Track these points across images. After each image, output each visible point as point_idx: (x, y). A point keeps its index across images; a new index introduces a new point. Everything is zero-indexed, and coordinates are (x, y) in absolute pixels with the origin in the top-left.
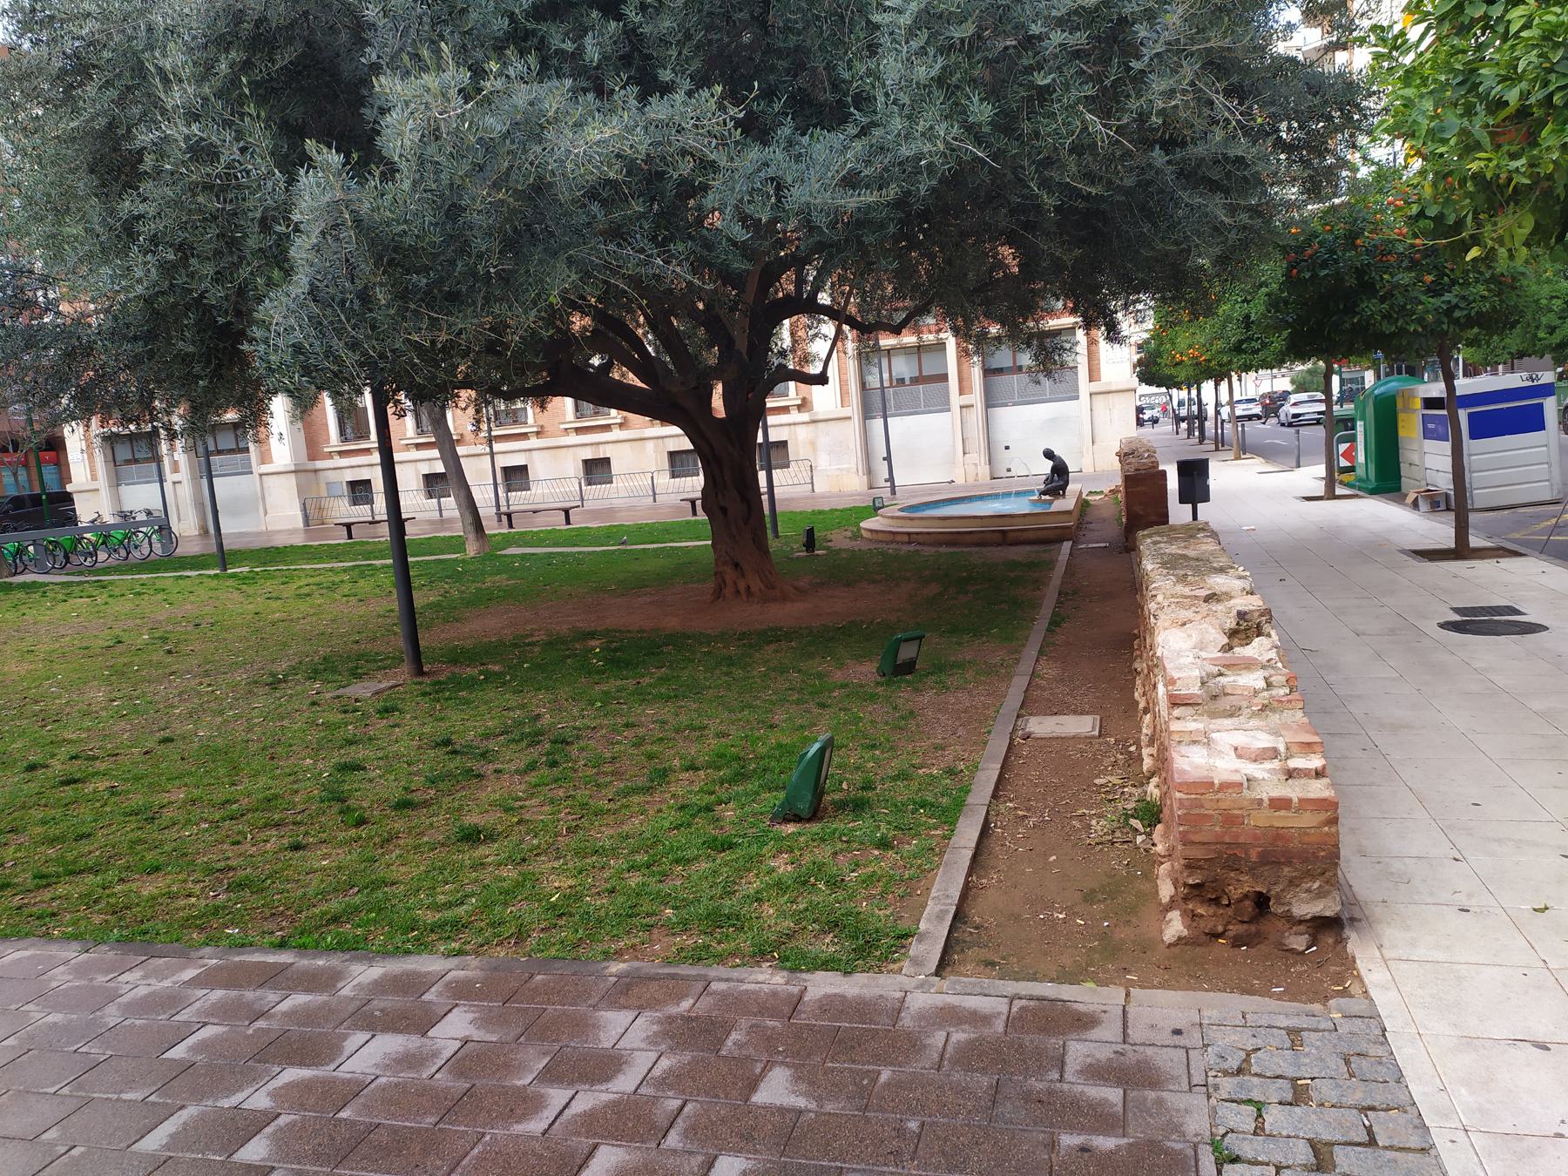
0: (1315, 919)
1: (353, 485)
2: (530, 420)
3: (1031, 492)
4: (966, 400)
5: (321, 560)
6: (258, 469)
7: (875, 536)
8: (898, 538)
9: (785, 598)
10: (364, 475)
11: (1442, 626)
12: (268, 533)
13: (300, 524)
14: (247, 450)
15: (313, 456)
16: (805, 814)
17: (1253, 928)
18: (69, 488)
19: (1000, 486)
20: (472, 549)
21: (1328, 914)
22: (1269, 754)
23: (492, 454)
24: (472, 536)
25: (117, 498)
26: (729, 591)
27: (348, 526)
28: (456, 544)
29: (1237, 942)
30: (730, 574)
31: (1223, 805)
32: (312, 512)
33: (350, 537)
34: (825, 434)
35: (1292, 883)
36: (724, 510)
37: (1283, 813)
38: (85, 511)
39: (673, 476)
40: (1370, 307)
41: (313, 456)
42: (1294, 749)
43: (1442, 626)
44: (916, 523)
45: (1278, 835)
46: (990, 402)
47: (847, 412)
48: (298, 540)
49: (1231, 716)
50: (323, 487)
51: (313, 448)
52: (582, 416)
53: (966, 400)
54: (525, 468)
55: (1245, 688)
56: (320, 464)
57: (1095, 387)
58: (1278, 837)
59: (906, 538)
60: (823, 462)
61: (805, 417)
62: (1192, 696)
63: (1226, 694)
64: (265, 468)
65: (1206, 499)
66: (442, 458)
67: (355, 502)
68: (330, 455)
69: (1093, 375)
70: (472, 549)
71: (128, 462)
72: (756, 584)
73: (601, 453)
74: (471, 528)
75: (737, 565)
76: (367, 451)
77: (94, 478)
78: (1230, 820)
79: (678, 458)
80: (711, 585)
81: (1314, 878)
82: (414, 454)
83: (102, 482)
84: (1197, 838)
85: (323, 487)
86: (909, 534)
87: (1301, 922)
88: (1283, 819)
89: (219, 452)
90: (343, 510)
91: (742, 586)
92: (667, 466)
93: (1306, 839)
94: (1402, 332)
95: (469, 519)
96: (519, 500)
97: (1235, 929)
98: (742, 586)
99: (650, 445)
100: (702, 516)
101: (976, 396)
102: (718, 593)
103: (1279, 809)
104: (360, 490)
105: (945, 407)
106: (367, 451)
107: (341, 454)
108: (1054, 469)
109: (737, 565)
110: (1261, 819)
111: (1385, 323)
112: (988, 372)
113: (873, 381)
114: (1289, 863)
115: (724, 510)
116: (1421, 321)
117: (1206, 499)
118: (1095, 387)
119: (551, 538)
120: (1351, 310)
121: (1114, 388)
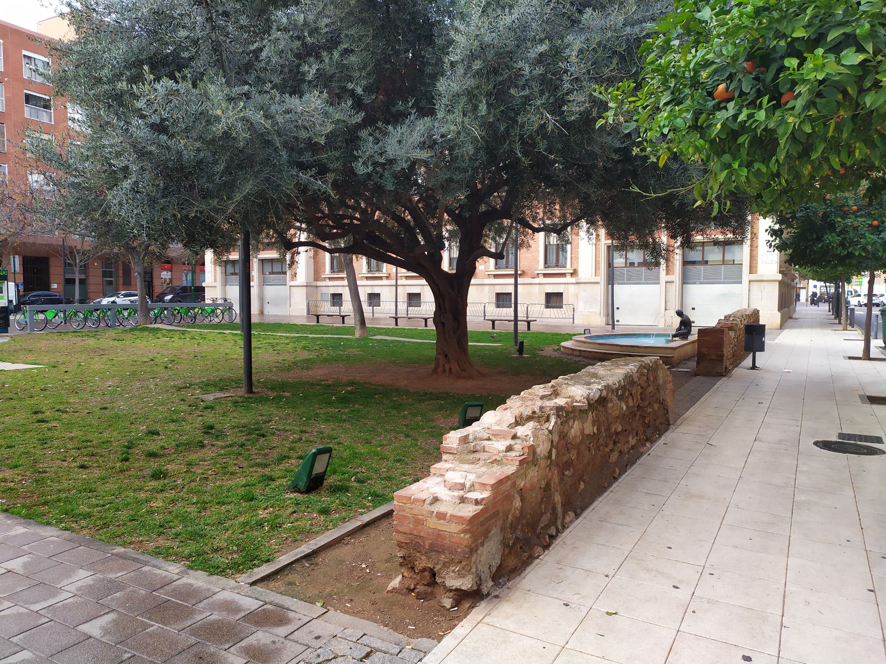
0: (457, 590)
1: (334, 296)
2: (384, 271)
3: (669, 335)
4: (670, 278)
5: (289, 331)
6: (290, 283)
7: (567, 351)
8: (575, 353)
9: (470, 377)
10: (338, 291)
11: (816, 443)
12: (290, 316)
13: (305, 314)
14: (285, 273)
15: (316, 279)
16: (302, 489)
17: (429, 590)
18: (204, 285)
19: (616, 332)
20: (358, 334)
21: (464, 588)
22: (459, 487)
23: (396, 286)
24: (358, 327)
25: (225, 292)
26: (440, 369)
27: (493, 322)
28: (350, 331)
29: (419, 597)
30: (442, 360)
31: (415, 512)
32: (312, 308)
33: (397, 324)
34: (585, 292)
35: (445, 565)
36: (443, 324)
37: (442, 521)
38: (209, 295)
39: (498, 306)
40: (831, 238)
41: (316, 279)
42: (477, 486)
43: (816, 443)
44: (586, 345)
45: (439, 534)
46: (685, 280)
47: (597, 279)
48: (304, 322)
49: (473, 463)
50: (319, 295)
51: (317, 274)
52: (499, 268)
53: (670, 278)
54: (419, 294)
55: (495, 449)
56: (319, 283)
57: (753, 277)
58: (439, 536)
59: (578, 353)
60: (581, 307)
61: (573, 280)
62: (451, 448)
63: (484, 451)
64: (293, 283)
65: (762, 349)
66: (349, 286)
67: (334, 305)
68: (324, 279)
69: (752, 269)
70: (358, 334)
71: (232, 274)
72: (455, 367)
73: (376, 290)
74: (358, 323)
75: (446, 356)
76: (342, 278)
77: (215, 281)
78: (418, 522)
79: (501, 297)
80: (433, 366)
81: (456, 564)
82: (365, 282)
83: (218, 283)
84: (401, 529)
85: (319, 295)
86: (580, 351)
87: (451, 591)
88: (442, 526)
89: (273, 273)
90: (327, 308)
91: (447, 368)
92: (543, 302)
93: (452, 540)
94: (850, 255)
95: (358, 318)
96: (414, 311)
97: (421, 588)
98: (447, 368)
99: (487, 288)
100: (432, 326)
101: (676, 276)
102: (435, 371)
103: (440, 519)
104: (337, 298)
105: (656, 281)
106: (342, 278)
107: (330, 279)
108: (682, 323)
109: (446, 356)
110: (432, 523)
111: (840, 249)
112: (686, 263)
113: (619, 261)
114: (444, 553)
115: (443, 324)
116: (864, 249)
117: (762, 349)
118: (753, 277)
119: (387, 332)
120: (819, 239)
121: (765, 279)
